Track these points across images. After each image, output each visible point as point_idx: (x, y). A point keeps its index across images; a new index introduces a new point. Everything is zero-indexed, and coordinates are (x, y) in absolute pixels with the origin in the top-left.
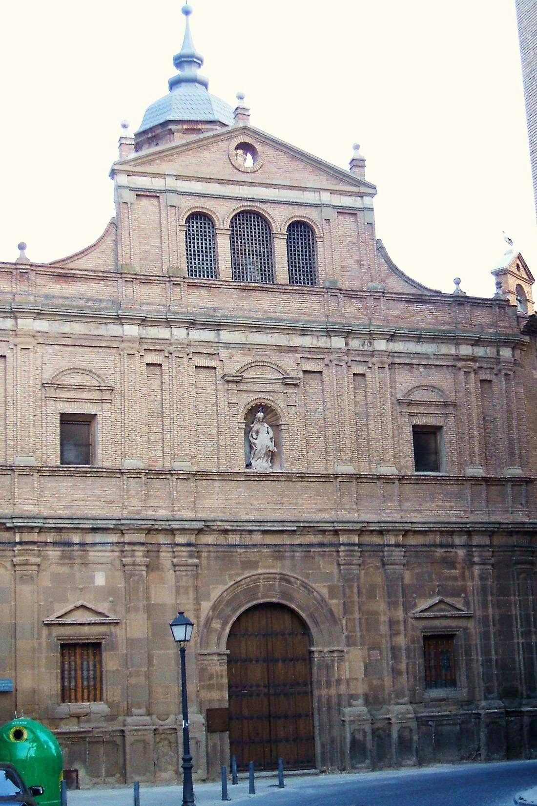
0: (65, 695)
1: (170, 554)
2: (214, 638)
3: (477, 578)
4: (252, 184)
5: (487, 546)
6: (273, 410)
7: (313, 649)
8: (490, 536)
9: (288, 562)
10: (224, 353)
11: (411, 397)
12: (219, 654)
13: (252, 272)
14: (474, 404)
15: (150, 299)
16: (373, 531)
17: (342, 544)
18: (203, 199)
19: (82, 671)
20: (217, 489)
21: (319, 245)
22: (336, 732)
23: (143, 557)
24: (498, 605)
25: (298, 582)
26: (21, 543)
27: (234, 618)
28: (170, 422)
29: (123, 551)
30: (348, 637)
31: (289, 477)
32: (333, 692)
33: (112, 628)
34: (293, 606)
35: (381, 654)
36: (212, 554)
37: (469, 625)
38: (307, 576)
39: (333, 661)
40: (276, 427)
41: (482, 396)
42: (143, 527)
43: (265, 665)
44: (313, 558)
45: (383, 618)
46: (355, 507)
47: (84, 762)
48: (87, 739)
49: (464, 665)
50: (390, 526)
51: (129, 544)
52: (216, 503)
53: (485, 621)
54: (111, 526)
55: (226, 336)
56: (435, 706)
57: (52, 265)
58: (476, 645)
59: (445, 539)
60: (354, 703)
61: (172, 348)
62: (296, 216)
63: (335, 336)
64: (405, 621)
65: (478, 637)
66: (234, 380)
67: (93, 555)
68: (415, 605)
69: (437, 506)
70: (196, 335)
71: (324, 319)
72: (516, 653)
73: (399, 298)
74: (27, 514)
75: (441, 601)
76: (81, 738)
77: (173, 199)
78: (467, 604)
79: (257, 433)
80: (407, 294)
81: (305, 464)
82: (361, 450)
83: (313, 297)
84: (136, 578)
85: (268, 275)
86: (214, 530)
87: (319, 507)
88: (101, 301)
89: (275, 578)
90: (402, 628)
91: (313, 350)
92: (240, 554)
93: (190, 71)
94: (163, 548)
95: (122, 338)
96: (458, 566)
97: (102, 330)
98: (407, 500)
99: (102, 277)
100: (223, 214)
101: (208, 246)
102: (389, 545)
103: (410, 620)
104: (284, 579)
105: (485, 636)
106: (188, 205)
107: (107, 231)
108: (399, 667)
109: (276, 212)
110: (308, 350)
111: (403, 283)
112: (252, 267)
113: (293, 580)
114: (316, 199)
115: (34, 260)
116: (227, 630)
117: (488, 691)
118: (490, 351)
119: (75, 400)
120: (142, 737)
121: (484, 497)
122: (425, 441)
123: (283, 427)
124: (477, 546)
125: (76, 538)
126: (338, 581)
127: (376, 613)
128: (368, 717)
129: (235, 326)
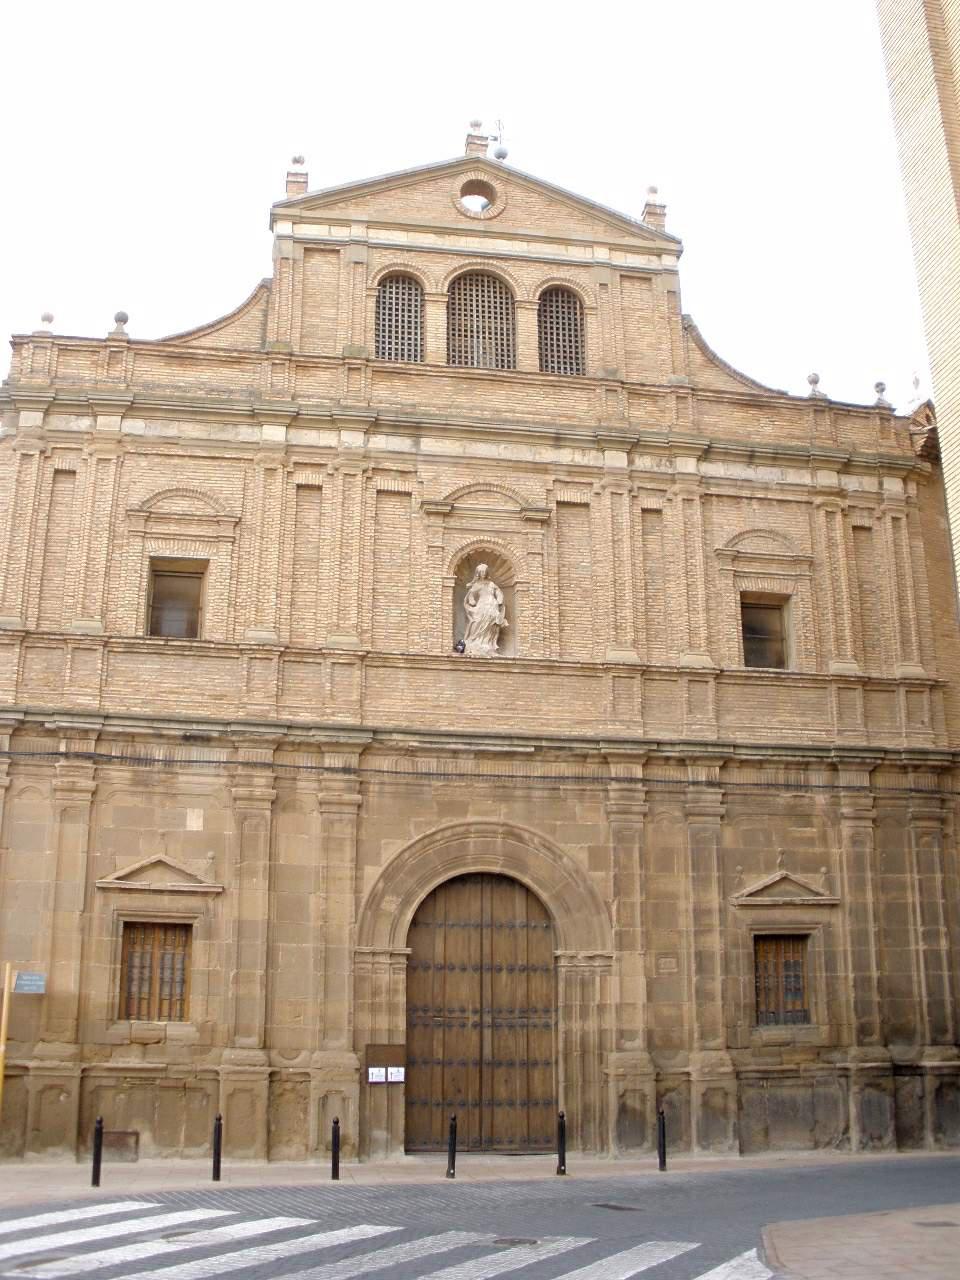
0: (127, 1008)
1: (315, 785)
2: (384, 927)
3: (846, 842)
4: (486, 234)
5: (864, 788)
6: (505, 561)
7: (559, 952)
8: (871, 772)
9: (519, 806)
11: (739, 547)
12: (392, 955)
13: (477, 347)
14: (842, 561)
15: (317, 388)
16: (668, 759)
18: (406, 254)
19: (162, 969)
20: (401, 682)
22: (594, 1095)
23: (267, 786)
24: (881, 887)
25: (536, 840)
26: (66, 755)
27: (422, 896)
28: (335, 578)
29: (233, 776)
30: (620, 935)
31: (527, 667)
32: (592, 1025)
33: (210, 901)
34: (526, 880)
35: (678, 964)
36: (387, 788)
37: (833, 920)
38: (553, 830)
39: (593, 973)
40: (506, 587)
41: (854, 552)
42: (267, 737)
43: (477, 976)
44: (565, 800)
45: (685, 905)
46: (638, 718)
47: (151, 1121)
48: (158, 1082)
49: (823, 986)
50: (698, 751)
51: (246, 764)
52: (398, 703)
53: (858, 913)
54: (215, 735)
55: (429, 445)
56: (771, 1055)
57: (165, 342)
58: (845, 952)
59: (793, 776)
60: (628, 1045)
62: (553, 279)
63: (610, 449)
64: (722, 911)
65: (849, 939)
66: (444, 511)
67: (185, 780)
68: (741, 884)
69: (781, 722)
70: (380, 442)
71: (593, 423)
72: (914, 968)
73: (718, 397)
74: (78, 709)
75: (784, 879)
76: (146, 1079)
77: (361, 254)
78: (830, 884)
79: (477, 597)
80: (731, 393)
81: (555, 647)
82: (649, 630)
83: (578, 393)
84: (254, 822)
85: (506, 357)
86: (391, 748)
87: (577, 717)
88: (231, 392)
89: (495, 832)
90: (716, 920)
91: (574, 470)
92: (437, 789)
94: (303, 774)
95: (256, 446)
96: (815, 820)
97: (229, 434)
98: (729, 711)
99: (235, 358)
100: (436, 276)
101: (413, 320)
102: (695, 783)
103: (732, 909)
104: (511, 833)
105: (860, 938)
106: (382, 261)
107: (254, 297)
108: (709, 986)
109: (521, 273)
110: (565, 468)
111: (726, 378)
112: (481, 348)
113: (526, 836)
114: (585, 261)
115: (133, 336)
116: (409, 916)
117: (863, 1031)
118: (869, 483)
119: (174, 537)
120: (249, 1086)
121: (860, 710)
122: (760, 622)
123: (518, 587)
124: (847, 788)
125: (159, 753)
126: (607, 840)
127: (674, 896)
128: (650, 1069)
129: (444, 430)
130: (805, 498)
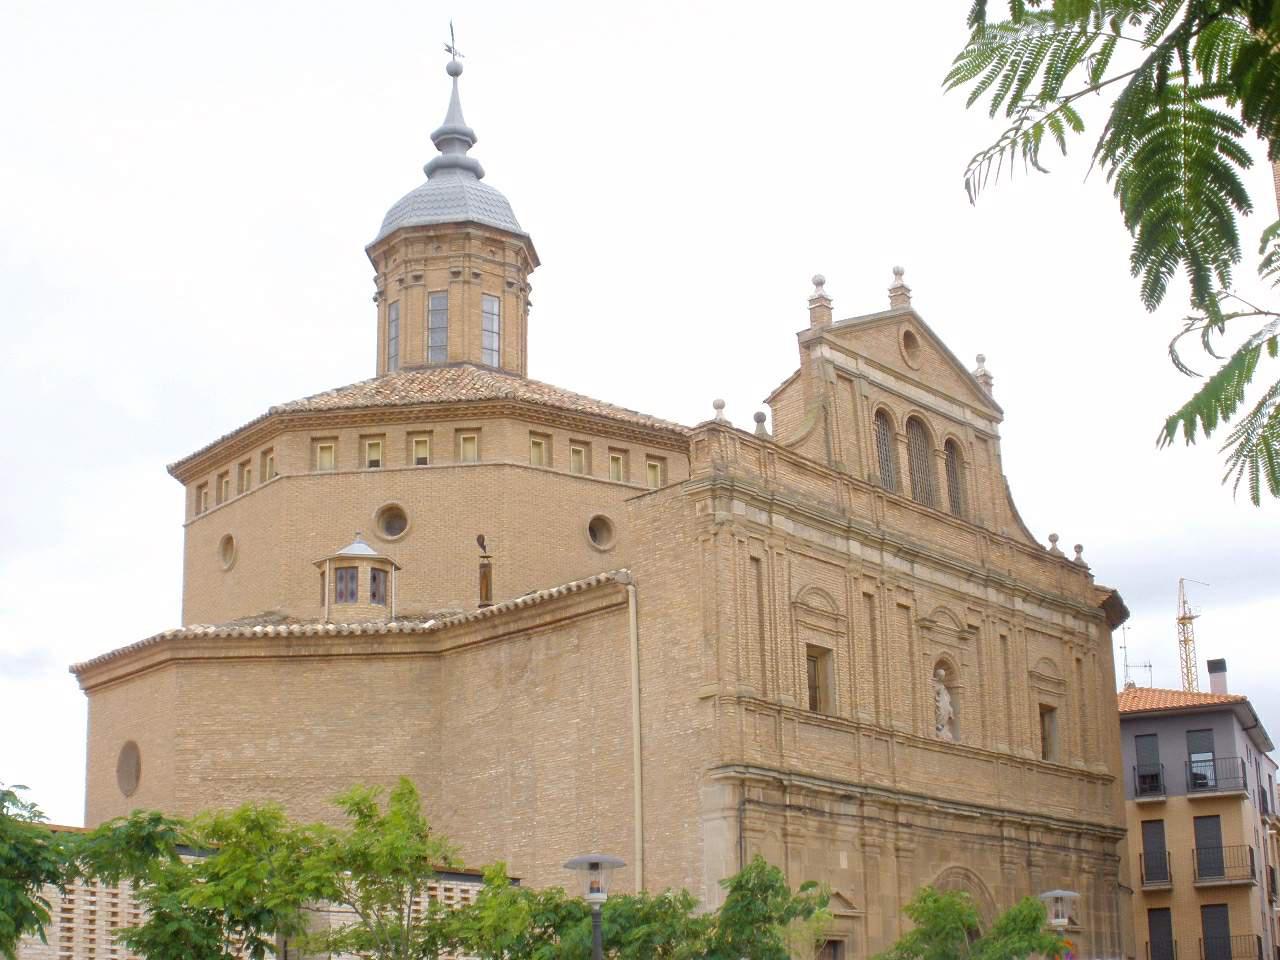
10: (919, 592)
17: (1006, 839)
21: (967, 472)
55: (921, 571)
61: (885, 577)
77: (867, 389)
91: (978, 601)
93: (457, 154)
130: (1059, 635)
